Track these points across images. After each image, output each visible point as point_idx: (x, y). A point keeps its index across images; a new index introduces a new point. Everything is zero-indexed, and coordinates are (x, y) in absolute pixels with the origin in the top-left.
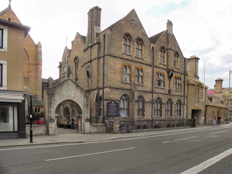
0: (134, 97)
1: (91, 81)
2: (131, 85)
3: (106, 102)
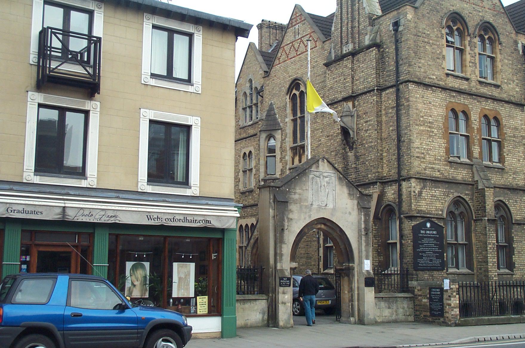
0: (485, 207)
1: (357, 158)
2: (472, 169)
3: (409, 225)
